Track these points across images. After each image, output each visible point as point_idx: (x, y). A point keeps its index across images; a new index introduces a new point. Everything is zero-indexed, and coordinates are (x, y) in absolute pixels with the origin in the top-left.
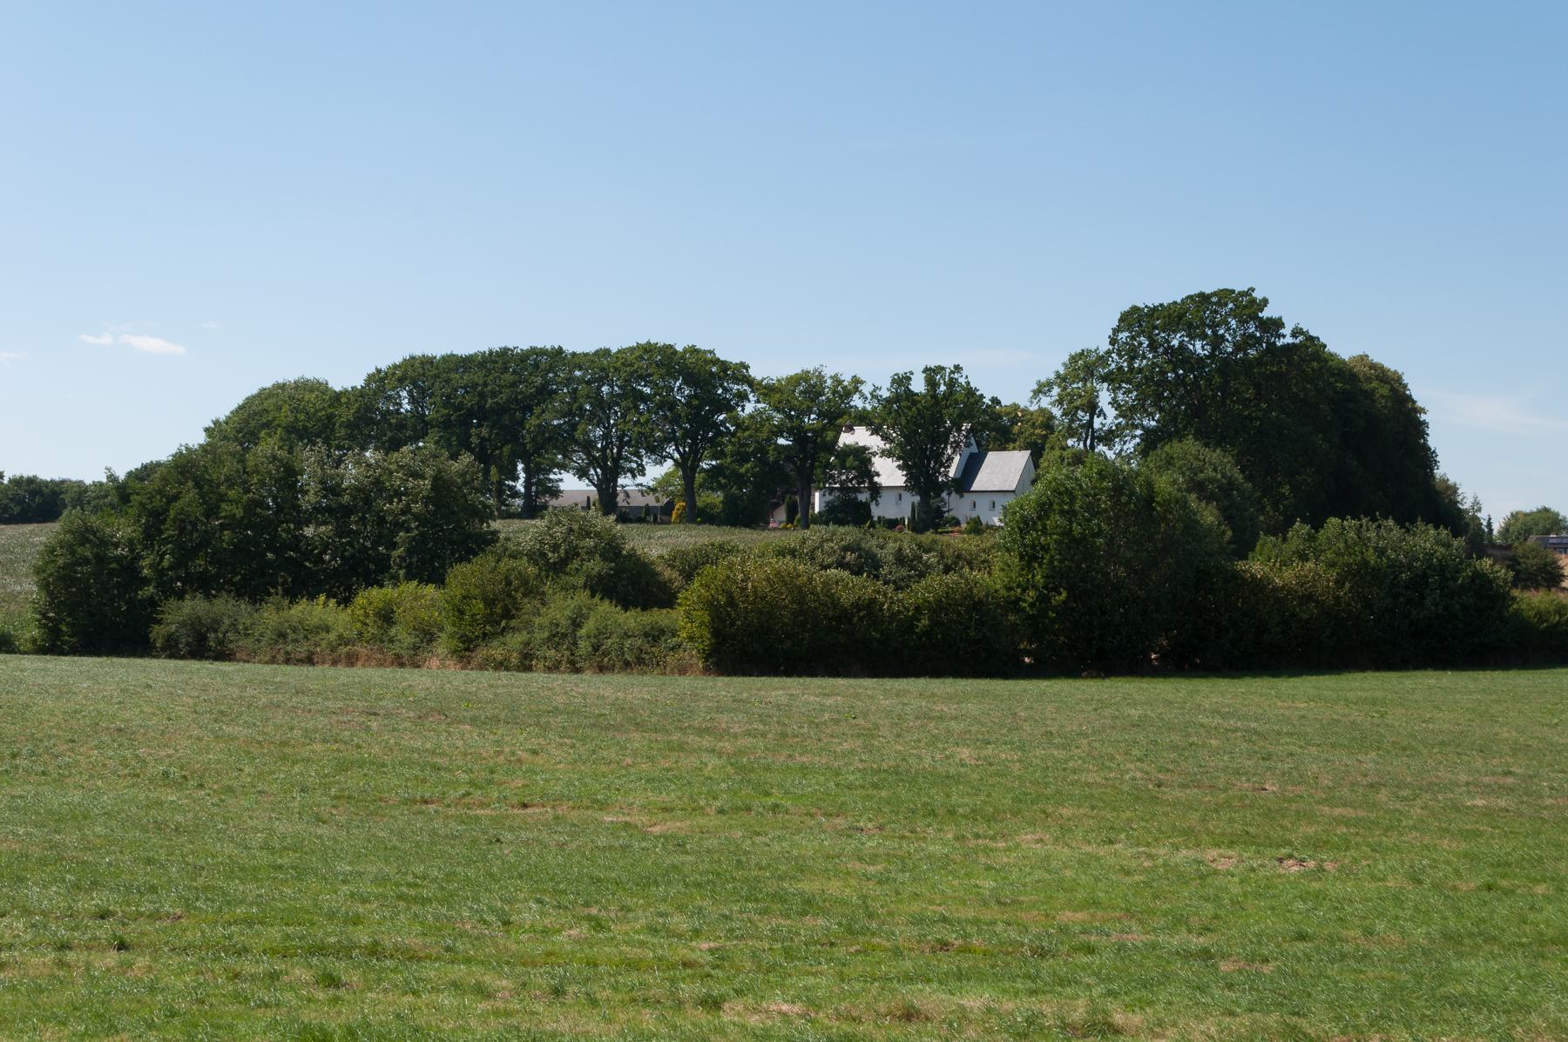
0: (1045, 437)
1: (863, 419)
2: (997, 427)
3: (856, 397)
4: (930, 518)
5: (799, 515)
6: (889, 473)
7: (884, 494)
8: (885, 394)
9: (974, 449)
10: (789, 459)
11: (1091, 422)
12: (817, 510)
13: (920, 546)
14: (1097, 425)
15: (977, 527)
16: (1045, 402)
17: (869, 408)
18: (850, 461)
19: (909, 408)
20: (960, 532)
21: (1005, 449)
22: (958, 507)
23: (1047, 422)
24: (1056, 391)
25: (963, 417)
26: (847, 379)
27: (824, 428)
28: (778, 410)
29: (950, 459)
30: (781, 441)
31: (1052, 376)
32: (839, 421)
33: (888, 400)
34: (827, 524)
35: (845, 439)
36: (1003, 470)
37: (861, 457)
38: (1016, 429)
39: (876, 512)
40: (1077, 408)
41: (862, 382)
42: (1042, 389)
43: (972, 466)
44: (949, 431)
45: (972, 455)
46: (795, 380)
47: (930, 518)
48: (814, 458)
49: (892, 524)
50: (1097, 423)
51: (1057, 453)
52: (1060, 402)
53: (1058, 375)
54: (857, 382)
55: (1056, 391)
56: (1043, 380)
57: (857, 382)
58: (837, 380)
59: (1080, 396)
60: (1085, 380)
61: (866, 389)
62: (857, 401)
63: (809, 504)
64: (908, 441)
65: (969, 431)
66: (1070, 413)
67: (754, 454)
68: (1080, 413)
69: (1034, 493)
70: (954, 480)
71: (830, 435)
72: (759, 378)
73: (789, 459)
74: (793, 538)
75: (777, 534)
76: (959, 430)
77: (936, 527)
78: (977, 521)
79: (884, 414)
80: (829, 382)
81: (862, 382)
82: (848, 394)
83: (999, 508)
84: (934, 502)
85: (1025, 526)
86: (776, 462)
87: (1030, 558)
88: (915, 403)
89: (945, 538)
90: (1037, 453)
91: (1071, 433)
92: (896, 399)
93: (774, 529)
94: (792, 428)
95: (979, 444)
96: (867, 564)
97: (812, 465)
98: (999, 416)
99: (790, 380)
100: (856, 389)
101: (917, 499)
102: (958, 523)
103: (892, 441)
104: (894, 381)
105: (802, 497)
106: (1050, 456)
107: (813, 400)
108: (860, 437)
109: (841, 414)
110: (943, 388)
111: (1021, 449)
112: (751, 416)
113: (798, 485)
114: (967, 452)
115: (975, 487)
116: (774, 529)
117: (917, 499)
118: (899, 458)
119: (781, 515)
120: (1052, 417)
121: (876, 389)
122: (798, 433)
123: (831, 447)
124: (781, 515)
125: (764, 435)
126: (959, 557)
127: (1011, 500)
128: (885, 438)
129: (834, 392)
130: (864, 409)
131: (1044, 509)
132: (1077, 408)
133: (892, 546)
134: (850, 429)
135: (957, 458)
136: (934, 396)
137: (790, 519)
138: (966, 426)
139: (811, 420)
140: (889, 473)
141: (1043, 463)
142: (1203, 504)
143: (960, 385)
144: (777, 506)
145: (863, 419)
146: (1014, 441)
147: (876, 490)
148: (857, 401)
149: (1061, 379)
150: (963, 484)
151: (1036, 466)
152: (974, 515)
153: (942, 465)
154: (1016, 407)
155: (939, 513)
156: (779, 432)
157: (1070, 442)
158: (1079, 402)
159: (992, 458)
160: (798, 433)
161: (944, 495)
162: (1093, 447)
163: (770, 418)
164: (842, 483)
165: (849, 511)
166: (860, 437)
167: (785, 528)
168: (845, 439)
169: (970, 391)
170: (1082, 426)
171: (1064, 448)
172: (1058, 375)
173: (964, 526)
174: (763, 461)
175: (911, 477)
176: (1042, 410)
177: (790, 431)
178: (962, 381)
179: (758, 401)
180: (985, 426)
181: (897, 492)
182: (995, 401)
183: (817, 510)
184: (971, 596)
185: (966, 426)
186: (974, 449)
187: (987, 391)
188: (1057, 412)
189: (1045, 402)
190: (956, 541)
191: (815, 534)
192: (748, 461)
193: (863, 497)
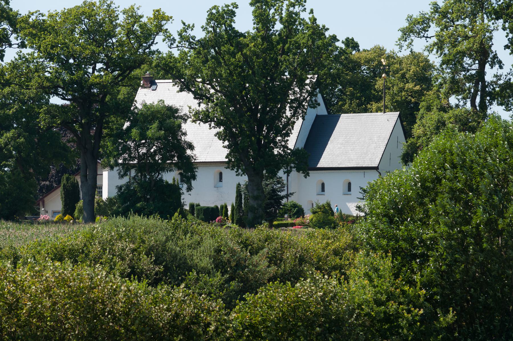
0: (420, 94)
1: (169, 69)
2: (352, 80)
3: (159, 38)
4: (262, 206)
5: (80, 202)
6: (206, 144)
7: (200, 173)
8: (199, 34)
9: (322, 110)
10: (66, 125)
11: (481, 73)
12: (105, 196)
13: (245, 244)
14: (489, 77)
15: (326, 218)
16: (419, 45)
17: (176, 53)
18: (153, 130)
19: (233, 55)
20: (303, 225)
21: (366, 111)
22: (301, 190)
23: (423, 76)
24: (434, 29)
25: (306, 66)
26: (146, 14)
27: (115, 82)
28: (51, 57)
29: (290, 124)
30: (55, 100)
31: (428, 10)
32: (137, 72)
33: (204, 44)
34: (125, 214)
35: (145, 98)
36: (362, 138)
37: (168, 119)
38: (379, 84)
39: (188, 199)
40: (463, 54)
41: (169, 19)
42: (415, 27)
43: (320, 134)
44: (288, 86)
45: (318, 118)
46: (74, 16)
47: (262, 206)
48: (101, 124)
49: (210, 214)
50: (490, 73)
51: (434, 115)
52: (440, 45)
53: (436, 8)
54: (160, 17)
55: (434, 29)
56: (416, 15)
57: (160, 17)
58: (133, 16)
59: (466, 37)
60: (473, 15)
61: (173, 28)
62: (160, 45)
63: (95, 188)
64: (230, 97)
65: (314, 86)
66: (454, 62)
67: (16, 116)
68: (467, 60)
69: (409, 172)
70: (295, 152)
71: (123, 91)
72: (23, 13)
73: (66, 125)
74: (76, 233)
75: (50, 229)
76: (301, 84)
77: (270, 218)
78: (326, 210)
79: (198, 63)
80: (121, 19)
81: (169, 19)
82: (147, 36)
83: (356, 190)
84: (268, 185)
85: (395, 213)
86: (49, 128)
87: (407, 255)
88: (240, 47)
89: (285, 234)
90: (408, 116)
91: (456, 88)
92: (213, 42)
93: (47, 223)
94: (72, 82)
95: (328, 104)
96: (172, 269)
97: (99, 133)
98: (356, 65)
99: (67, 14)
100: (159, 28)
101: (244, 179)
102: (300, 212)
103: (209, 99)
104: (211, 17)
105: (85, 178)
106: (426, 120)
107: (99, 44)
108: (165, 94)
109: (138, 63)
110: (278, 26)
111: (384, 109)
112: (14, 66)
113: (80, 161)
114: (312, 114)
115: (323, 163)
116: (47, 223)
117: (244, 179)
118: (218, 124)
119: (55, 202)
120: (428, 66)
121: (187, 27)
122: (82, 93)
123: (125, 108)
124: (55, 202)
125: (32, 92)
126: (302, 260)
127: (373, 178)
128: (199, 96)
129: (130, 32)
130: (170, 55)
131: (428, 188)
132: (463, 54)
133: (209, 243)
134: (151, 83)
135: (299, 123)
136: (267, 38)
137: (69, 208)
138: (311, 79)
139: (97, 72)
140: (206, 144)
141: (417, 130)
142: (188, 310)
143: (302, 22)
144: (50, 190)
145: (169, 69)
146: (378, 99)
147: (189, 169)
148: (160, 45)
149: (442, 14)
150: (306, 159)
151: (408, 134)
152: (322, 201)
153: (278, 132)
154: (380, 52)
155: (275, 199)
156: (52, 89)
157: (453, 100)
158: (464, 45)
159: (348, 124)
160: (82, 93)
161: (281, 173)
162: (484, 107)
163: (40, 69)
164: (140, 158)
165: (153, 197)
166: (165, 94)
167: (61, 221)
168: (145, 98)
169: (317, 32)
170: (469, 79)
171: (444, 109)
172: (436, 8)
173: (309, 216)
174: (30, 129)
175: (235, 149)
176: (414, 56)
177: (67, 86)
178: (305, 16)
179: (23, 45)
180: (336, 78)
181: (216, 170)
182: (351, 44)
183: (105, 196)
184: (326, 314)
185: (311, 79)
186: (322, 110)
187: (339, 27)
188: (435, 59)
189: (419, 45)
190: (300, 237)
191: (102, 226)
192: (8, 129)
193: (170, 177)
